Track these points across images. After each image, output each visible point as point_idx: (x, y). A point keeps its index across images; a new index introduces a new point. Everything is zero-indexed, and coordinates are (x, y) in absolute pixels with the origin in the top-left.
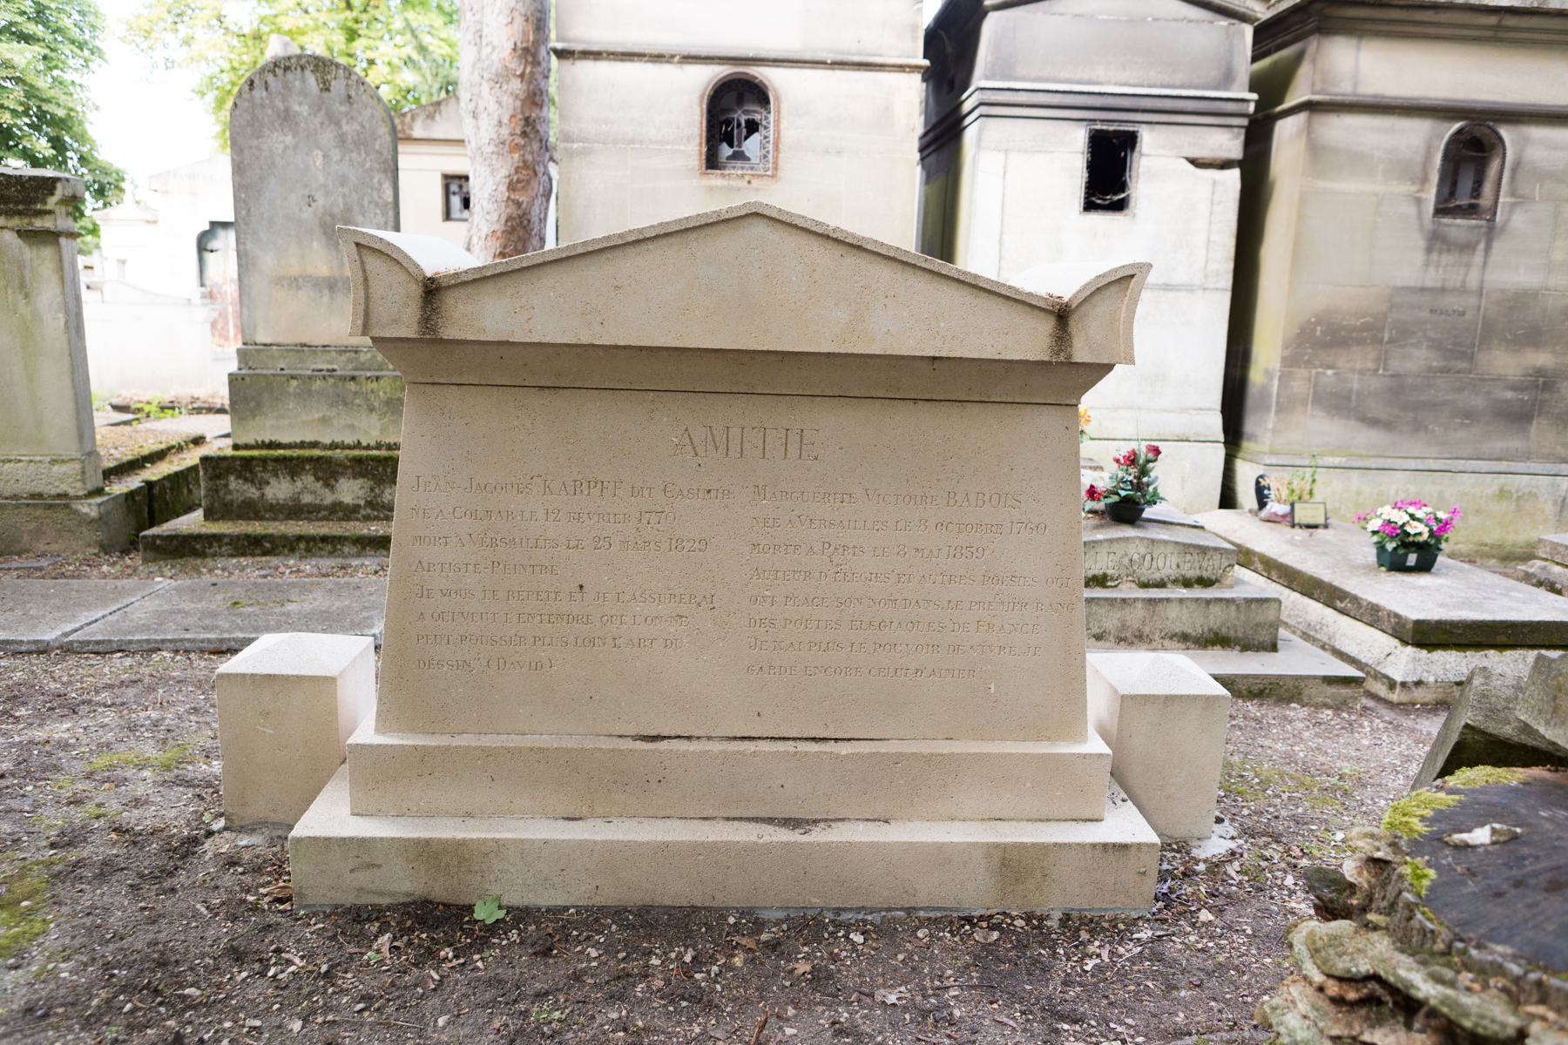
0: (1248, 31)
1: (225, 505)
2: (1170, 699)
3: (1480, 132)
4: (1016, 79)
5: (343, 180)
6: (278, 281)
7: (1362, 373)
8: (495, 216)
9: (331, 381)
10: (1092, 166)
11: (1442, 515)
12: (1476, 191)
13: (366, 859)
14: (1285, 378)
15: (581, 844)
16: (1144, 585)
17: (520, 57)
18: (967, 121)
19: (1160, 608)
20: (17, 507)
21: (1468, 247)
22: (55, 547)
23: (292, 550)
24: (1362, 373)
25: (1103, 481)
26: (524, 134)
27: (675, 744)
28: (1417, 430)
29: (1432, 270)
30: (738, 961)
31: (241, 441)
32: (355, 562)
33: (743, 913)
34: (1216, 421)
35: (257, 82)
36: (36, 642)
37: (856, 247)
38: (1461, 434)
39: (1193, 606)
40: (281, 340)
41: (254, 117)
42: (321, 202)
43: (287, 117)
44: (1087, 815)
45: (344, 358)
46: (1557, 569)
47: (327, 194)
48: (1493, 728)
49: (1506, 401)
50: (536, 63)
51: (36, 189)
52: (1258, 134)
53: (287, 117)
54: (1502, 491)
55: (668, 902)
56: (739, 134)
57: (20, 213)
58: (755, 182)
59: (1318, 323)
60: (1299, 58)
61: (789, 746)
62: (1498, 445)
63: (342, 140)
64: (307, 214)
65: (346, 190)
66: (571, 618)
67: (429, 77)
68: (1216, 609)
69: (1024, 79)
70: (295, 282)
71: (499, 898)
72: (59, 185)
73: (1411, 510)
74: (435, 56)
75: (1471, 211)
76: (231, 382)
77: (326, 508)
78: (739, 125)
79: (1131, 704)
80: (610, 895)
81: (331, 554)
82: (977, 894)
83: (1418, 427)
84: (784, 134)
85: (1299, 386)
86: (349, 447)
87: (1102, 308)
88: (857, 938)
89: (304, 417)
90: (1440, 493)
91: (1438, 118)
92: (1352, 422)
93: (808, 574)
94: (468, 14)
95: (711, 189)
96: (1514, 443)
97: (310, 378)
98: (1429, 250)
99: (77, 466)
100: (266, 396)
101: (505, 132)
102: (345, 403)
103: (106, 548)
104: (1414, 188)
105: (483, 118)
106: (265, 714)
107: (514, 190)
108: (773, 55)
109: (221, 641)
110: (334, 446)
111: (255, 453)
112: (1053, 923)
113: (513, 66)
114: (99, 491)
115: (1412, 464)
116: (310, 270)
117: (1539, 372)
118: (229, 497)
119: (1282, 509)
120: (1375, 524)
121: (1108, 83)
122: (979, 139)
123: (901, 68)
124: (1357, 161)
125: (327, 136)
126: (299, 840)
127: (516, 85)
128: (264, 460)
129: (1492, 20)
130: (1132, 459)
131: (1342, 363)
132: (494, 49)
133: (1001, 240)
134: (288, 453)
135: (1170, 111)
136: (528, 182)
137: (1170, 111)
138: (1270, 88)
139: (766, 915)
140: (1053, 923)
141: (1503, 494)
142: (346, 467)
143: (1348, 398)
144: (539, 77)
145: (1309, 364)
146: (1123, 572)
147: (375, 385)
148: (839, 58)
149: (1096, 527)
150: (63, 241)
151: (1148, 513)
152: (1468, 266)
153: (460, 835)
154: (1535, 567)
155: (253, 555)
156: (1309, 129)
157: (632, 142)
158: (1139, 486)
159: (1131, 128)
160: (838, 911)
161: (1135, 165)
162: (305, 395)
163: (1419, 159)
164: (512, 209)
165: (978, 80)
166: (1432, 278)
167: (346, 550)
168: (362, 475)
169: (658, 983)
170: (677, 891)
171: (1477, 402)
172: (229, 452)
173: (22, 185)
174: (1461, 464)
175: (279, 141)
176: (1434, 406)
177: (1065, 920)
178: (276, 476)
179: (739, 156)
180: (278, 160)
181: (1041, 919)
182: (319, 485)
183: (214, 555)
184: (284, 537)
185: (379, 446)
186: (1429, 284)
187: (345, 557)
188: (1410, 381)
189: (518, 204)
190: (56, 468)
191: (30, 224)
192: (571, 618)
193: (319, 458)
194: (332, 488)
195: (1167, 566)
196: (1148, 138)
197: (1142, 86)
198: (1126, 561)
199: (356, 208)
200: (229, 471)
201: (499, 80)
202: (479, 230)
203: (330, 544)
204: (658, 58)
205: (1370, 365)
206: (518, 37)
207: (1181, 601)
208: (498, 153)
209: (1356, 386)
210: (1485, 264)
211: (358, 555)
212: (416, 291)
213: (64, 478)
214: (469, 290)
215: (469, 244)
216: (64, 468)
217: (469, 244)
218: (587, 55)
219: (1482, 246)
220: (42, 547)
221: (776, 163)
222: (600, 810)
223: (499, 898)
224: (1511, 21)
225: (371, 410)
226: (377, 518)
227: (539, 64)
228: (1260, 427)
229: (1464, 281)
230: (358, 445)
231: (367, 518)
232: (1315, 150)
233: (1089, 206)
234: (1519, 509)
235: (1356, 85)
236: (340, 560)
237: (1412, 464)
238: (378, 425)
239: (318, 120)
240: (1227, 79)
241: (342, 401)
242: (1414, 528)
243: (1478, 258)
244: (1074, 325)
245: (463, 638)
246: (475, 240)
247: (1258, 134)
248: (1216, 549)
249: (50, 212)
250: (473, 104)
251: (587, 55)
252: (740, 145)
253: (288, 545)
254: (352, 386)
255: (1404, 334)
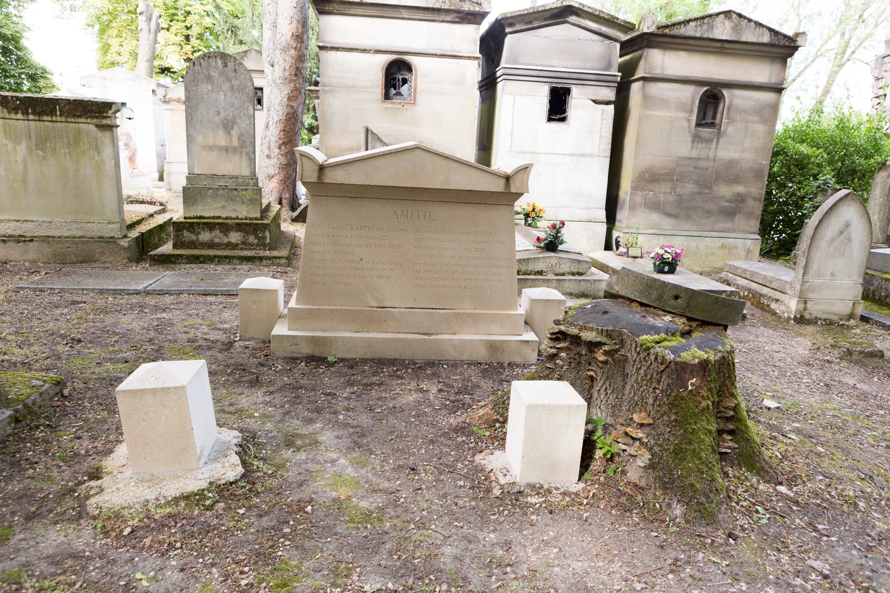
0: (618, 45)
1: (182, 243)
2: (547, 301)
3: (716, 91)
4: (519, 64)
5: (232, 105)
6: (204, 147)
7: (665, 193)
8: (281, 113)
9: (226, 190)
10: (551, 102)
11: (678, 251)
12: (714, 117)
13: (295, 342)
14: (632, 195)
15: (361, 338)
16: (557, 275)
17: (295, 39)
18: (499, 80)
19: (562, 283)
20: (94, 242)
21: (709, 141)
22: (110, 259)
23: (212, 261)
24: (665, 193)
25: (543, 235)
26: (296, 75)
27: (389, 309)
28: (688, 218)
29: (694, 149)
30: (410, 371)
31: (188, 216)
32: (239, 267)
33: (410, 361)
34: (602, 214)
35: (196, 63)
36: (135, 290)
37: (447, 158)
38: (706, 221)
39: (574, 282)
40: (204, 173)
41: (195, 77)
42: (223, 114)
43: (209, 78)
44: (517, 333)
45: (231, 181)
46: (731, 275)
47: (225, 111)
48: (611, 291)
49: (725, 207)
50: (302, 42)
51: (104, 107)
52: (623, 90)
53: (209, 78)
54: (723, 245)
55: (387, 357)
56: (399, 84)
57: (97, 117)
58: (405, 106)
59: (646, 172)
60: (640, 57)
61: (425, 310)
62: (722, 226)
63: (232, 88)
64: (217, 119)
65: (233, 109)
66: (358, 269)
67: (222, 23)
68: (583, 283)
69: (523, 64)
70: (211, 148)
71: (335, 355)
72: (113, 106)
73: (666, 249)
74: (226, 12)
75: (712, 125)
76: (183, 190)
77: (224, 244)
78: (399, 80)
79: (534, 302)
80: (369, 355)
81: (228, 263)
82: (482, 354)
83: (688, 217)
84: (418, 82)
85: (638, 199)
86: (234, 219)
87: (519, 177)
88: (446, 367)
89: (215, 206)
90: (697, 246)
91: (697, 85)
92: (661, 215)
93: (431, 256)
94: (268, 15)
95: (387, 108)
96: (728, 225)
97: (217, 189)
98: (693, 142)
99: (119, 225)
100: (198, 196)
101: (287, 73)
102: (232, 200)
103: (130, 260)
104: (687, 115)
105: (276, 66)
106: (254, 302)
107: (290, 101)
108: (414, 51)
109: (206, 290)
110: (227, 218)
111: (195, 220)
112: (506, 364)
113: (291, 43)
114: (126, 236)
115: (685, 233)
116: (217, 143)
117: (739, 195)
118: (183, 239)
119: (624, 250)
120: (652, 255)
121: (558, 67)
122: (503, 89)
123: (469, 58)
124: (663, 103)
125: (226, 86)
126: (274, 336)
127: (293, 52)
128: (198, 224)
129: (719, 45)
130: (554, 227)
131: (656, 189)
132: (283, 35)
133: (512, 133)
134: (209, 221)
135: (582, 79)
136: (297, 97)
137: (582, 79)
138: (628, 70)
139: (417, 361)
140: (506, 364)
141: (723, 246)
142: (233, 227)
143: (659, 204)
144: (303, 48)
145: (643, 189)
146: (549, 270)
147: (245, 192)
148: (443, 53)
149: (540, 253)
150: (114, 129)
151: (560, 247)
152: (710, 148)
153: (324, 335)
154: (723, 275)
155: (196, 263)
156: (643, 89)
157: (352, 87)
158: (556, 237)
159: (567, 86)
160: (440, 361)
161: (570, 102)
162: (215, 196)
163: (689, 102)
164: (289, 110)
165: (503, 64)
166: (694, 154)
167: (235, 262)
168: (240, 231)
169: (387, 374)
170: (390, 354)
171: (713, 207)
172: (182, 220)
173: (98, 105)
174: (706, 234)
175: (205, 88)
176: (695, 208)
177: (509, 364)
178: (204, 230)
179: (399, 94)
180: (205, 96)
181: (502, 364)
182: (222, 234)
183: (179, 263)
184: (209, 256)
185: (246, 219)
186: (693, 156)
187: (234, 265)
188: (685, 197)
189: (292, 107)
190: (109, 226)
191: (101, 122)
192: (358, 269)
193: (222, 223)
194: (227, 236)
195: (565, 267)
196: (575, 91)
197: (573, 68)
198: (550, 265)
199: (238, 117)
200: (184, 228)
201: (284, 50)
202: (273, 119)
203: (228, 259)
204: (364, 51)
205: (668, 190)
206: (294, 30)
207: (570, 280)
208: (283, 84)
209: (662, 199)
210: (716, 148)
211: (240, 264)
212: (317, 168)
213: (113, 230)
214: (332, 168)
215: (267, 125)
216: (113, 226)
217: (267, 125)
218: (333, 48)
219: (715, 140)
220: (104, 259)
221: (415, 98)
222: (366, 330)
223: (335, 355)
224: (727, 45)
225: (243, 203)
226: (246, 249)
227: (303, 42)
228: (622, 215)
229: (708, 155)
230: (237, 218)
231: (242, 249)
232: (646, 97)
233: (550, 120)
234: (730, 253)
235: (663, 70)
236: (232, 266)
237: (685, 233)
238: (246, 209)
239: (222, 79)
240: (609, 66)
241: (231, 199)
242: (666, 256)
243: (714, 145)
244: (511, 181)
245: (324, 275)
246: (271, 123)
247: (623, 90)
248: (584, 261)
249: (109, 117)
250: (270, 57)
251: (333, 48)
252: (399, 89)
253: (211, 259)
254: (235, 193)
255: (682, 177)
